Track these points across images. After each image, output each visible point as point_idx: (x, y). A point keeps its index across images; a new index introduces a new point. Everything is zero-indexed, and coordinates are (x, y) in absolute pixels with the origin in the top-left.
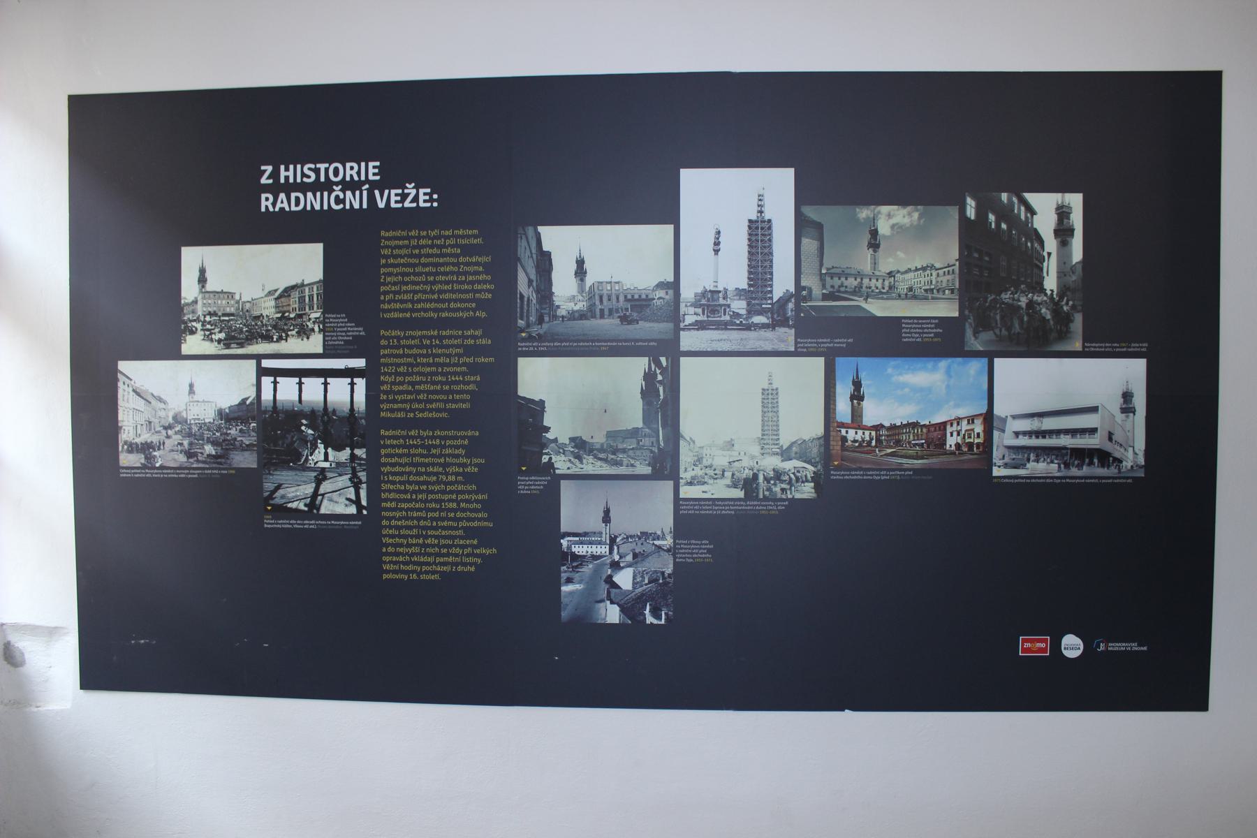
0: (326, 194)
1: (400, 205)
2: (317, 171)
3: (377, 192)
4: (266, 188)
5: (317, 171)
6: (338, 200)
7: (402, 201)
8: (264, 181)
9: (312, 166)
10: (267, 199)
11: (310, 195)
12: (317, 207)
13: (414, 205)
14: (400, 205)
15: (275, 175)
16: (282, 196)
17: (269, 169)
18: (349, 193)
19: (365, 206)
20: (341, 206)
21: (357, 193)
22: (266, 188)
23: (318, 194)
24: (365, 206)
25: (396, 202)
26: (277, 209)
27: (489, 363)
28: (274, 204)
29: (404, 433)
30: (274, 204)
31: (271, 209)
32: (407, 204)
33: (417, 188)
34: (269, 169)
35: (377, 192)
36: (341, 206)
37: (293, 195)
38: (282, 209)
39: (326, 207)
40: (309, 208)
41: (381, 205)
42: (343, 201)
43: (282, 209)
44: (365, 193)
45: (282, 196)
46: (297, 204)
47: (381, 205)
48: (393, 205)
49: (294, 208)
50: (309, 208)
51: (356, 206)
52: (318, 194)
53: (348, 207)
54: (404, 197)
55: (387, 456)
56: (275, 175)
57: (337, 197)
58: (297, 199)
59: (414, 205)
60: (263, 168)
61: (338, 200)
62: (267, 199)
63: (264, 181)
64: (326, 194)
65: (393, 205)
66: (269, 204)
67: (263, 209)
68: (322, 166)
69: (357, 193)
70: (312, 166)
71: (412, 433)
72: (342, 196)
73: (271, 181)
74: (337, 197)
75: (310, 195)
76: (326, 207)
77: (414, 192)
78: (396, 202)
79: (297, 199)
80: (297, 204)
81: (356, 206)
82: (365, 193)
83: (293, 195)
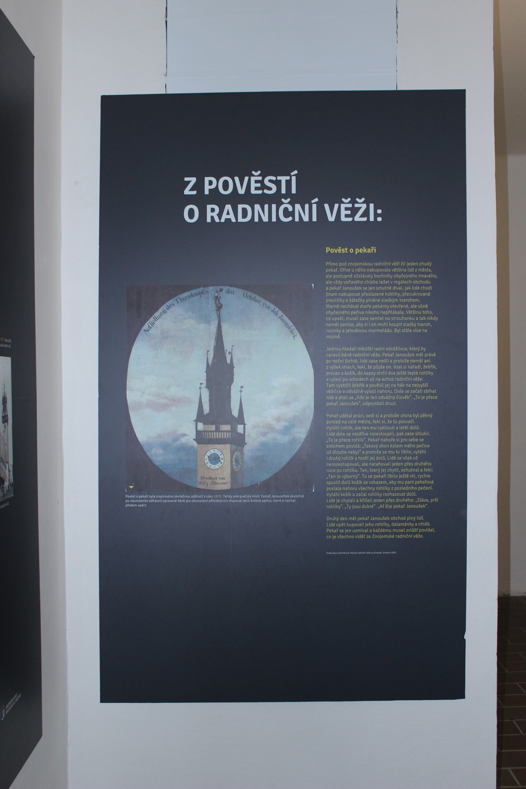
0: (274, 206)
1: (350, 219)
2: (278, 183)
3: (326, 206)
4: (190, 200)
5: (278, 183)
6: (287, 213)
7: (353, 215)
8: (187, 192)
9: (274, 178)
10: (213, 210)
11: (257, 207)
12: (265, 219)
13: (365, 219)
14: (350, 219)
15: (199, 186)
16: (228, 207)
17: (193, 180)
18: (298, 207)
19: (314, 219)
20: (290, 219)
21: (307, 206)
22: (190, 200)
23: (266, 206)
24: (314, 219)
25: (347, 216)
26: (223, 220)
27: (428, 490)
28: (220, 215)
29: (389, 264)
30: (220, 215)
31: (217, 220)
32: (357, 218)
33: (367, 202)
34: (193, 180)
35: (326, 206)
36: (290, 219)
37: (240, 207)
38: (228, 220)
39: (274, 219)
40: (256, 220)
41: (331, 218)
42: (292, 214)
43: (228, 220)
44: (314, 207)
45: (228, 207)
46: (245, 215)
47: (331, 218)
48: (343, 219)
49: (240, 220)
50: (256, 220)
51: (306, 219)
52: (266, 206)
53: (297, 219)
54: (354, 211)
55: (330, 425)
56: (199, 186)
57: (286, 209)
58: (245, 211)
59: (365, 219)
60: (186, 179)
61: (287, 213)
62: (213, 210)
63: (187, 192)
64: (274, 206)
65: (343, 219)
66: (215, 215)
67: (209, 220)
68: (283, 179)
69: (307, 206)
70: (274, 178)
71: (395, 264)
72: (290, 209)
73: (194, 193)
74: (286, 209)
75: (257, 207)
76: (274, 219)
77: (364, 206)
78: (347, 216)
79: (245, 211)
80: (245, 215)
81: (306, 219)
82: (314, 207)
83: (240, 207)
